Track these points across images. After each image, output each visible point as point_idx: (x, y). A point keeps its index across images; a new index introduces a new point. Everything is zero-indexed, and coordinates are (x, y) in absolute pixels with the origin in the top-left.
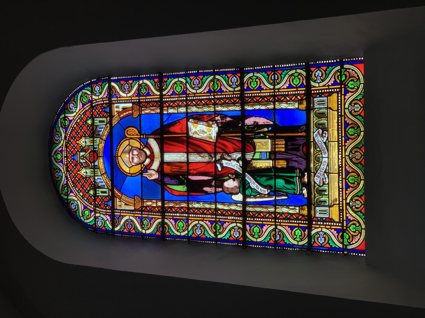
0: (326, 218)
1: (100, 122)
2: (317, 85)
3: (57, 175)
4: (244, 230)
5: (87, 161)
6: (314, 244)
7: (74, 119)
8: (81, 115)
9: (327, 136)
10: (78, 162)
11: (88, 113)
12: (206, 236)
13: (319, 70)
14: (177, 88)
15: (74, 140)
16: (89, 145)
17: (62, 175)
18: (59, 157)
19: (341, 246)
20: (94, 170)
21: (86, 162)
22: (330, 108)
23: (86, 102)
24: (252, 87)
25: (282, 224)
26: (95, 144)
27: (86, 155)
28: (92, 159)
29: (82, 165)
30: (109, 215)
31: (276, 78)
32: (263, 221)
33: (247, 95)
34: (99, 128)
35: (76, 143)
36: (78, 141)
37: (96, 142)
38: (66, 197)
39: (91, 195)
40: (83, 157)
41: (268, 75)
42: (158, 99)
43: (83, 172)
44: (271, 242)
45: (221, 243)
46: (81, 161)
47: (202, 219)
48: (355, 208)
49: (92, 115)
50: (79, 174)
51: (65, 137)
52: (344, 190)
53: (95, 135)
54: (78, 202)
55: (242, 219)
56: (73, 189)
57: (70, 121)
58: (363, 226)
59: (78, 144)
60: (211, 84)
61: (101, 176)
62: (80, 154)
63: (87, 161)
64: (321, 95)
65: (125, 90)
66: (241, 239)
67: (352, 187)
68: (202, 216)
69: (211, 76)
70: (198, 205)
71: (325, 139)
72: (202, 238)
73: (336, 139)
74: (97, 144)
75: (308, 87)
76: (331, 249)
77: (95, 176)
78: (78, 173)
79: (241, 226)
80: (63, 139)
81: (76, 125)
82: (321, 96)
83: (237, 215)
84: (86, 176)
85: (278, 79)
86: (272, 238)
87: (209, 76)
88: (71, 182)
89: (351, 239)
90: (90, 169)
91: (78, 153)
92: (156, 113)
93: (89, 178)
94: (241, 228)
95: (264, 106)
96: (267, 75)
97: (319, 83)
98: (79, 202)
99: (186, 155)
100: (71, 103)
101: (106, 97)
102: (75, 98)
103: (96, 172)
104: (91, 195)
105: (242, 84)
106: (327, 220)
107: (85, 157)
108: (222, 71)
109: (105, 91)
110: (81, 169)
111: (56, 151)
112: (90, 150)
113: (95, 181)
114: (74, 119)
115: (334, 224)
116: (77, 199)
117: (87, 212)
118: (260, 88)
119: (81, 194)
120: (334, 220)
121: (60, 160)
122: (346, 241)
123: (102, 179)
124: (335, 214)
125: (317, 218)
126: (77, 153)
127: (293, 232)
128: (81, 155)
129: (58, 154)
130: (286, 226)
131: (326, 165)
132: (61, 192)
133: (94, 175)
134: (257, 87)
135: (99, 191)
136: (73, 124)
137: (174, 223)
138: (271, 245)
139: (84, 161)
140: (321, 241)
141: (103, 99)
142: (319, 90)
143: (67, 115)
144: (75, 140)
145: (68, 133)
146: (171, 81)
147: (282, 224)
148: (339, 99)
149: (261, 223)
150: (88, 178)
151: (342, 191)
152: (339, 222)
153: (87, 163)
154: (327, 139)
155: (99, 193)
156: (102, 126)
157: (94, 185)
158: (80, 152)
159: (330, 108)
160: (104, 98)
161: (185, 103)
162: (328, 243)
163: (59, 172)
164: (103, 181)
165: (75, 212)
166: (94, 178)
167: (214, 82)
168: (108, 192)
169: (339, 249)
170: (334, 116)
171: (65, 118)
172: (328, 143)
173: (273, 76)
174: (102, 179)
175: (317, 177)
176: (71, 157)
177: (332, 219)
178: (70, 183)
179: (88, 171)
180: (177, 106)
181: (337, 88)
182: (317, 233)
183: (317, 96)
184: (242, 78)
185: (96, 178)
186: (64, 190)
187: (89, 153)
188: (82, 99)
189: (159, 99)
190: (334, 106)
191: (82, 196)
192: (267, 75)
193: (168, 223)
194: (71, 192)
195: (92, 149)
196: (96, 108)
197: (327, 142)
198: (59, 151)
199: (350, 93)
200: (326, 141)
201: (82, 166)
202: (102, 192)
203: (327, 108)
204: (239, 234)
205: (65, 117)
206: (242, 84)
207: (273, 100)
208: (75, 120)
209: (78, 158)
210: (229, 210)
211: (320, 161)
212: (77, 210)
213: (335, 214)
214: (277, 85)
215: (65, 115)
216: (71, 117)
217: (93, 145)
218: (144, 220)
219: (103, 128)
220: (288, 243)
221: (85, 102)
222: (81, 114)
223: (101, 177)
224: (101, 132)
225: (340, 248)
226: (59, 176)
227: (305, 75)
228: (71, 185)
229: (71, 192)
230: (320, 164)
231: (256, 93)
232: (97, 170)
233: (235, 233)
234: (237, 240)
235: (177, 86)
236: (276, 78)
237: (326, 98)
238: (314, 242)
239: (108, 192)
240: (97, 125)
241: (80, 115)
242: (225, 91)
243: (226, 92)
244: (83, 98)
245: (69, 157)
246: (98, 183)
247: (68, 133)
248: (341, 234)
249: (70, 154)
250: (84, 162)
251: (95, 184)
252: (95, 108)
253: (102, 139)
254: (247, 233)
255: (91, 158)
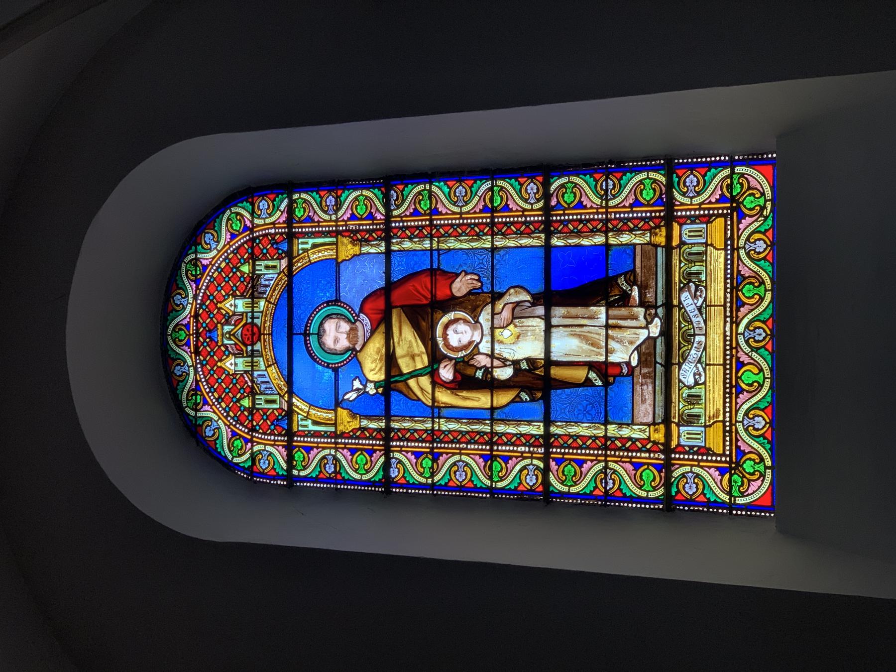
0: (700, 447)
1: (267, 267)
2: (687, 201)
3: (178, 371)
4: (546, 471)
5: (238, 342)
6: (596, 491)
7: (213, 263)
8: (228, 254)
9: (704, 296)
10: (219, 344)
11: (242, 250)
12: (624, 492)
13: (532, 182)
14: (359, 207)
15: (212, 301)
16: (243, 313)
17: (189, 370)
18: (182, 335)
19: (726, 498)
20: (252, 360)
21: (236, 344)
22: (712, 245)
23: (238, 231)
24: (645, 199)
25: (701, 464)
26: (255, 310)
27: (235, 330)
28: (248, 339)
29: (227, 348)
30: (283, 446)
31: (611, 187)
32: (373, 445)
33: (560, 217)
34: (265, 280)
35: (217, 307)
36: (221, 302)
37: (257, 307)
38: (192, 413)
39: (242, 408)
40: (230, 335)
41: (596, 181)
42: (540, 218)
43: (228, 364)
44: (597, 492)
45: (620, 504)
46: (226, 342)
47: (399, 449)
48: (753, 429)
49: (252, 254)
50: (221, 367)
51: (195, 297)
52: (734, 396)
53: (256, 294)
54: (220, 422)
55: (543, 451)
56: (210, 397)
57: (205, 267)
58: (769, 463)
59: (220, 309)
60: (488, 197)
61: (266, 370)
62: (222, 329)
63: (238, 342)
64: (694, 219)
65: (261, 212)
66: (541, 489)
67: (748, 392)
68: (316, 440)
69: (725, 168)
70: (529, 427)
71: (701, 300)
72: (269, 475)
73: (720, 302)
74: (258, 310)
75: (669, 204)
76: (709, 504)
77: (253, 370)
78: (219, 364)
79: (541, 465)
80: (191, 302)
81: (218, 272)
82: (693, 222)
83: (613, 447)
84: (235, 371)
85: (614, 188)
86: (599, 486)
87: (484, 181)
88: (205, 383)
89: (746, 486)
90: (243, 357)
91: (219, 325)
92: (517, 247)
93: (242, 375)
94: (541, 468)
95: (465, 244)
96: (319, 197)
97: (692, 198)
98: (222, 423)
99: (605, 331)
100: (208, 233)
101: (284, 222)
102: (216, 224)
103: (255, 364)
104: (242, 408)
105: (547, 196)
106: (702, 451)
107: (233, 335)
108: (704, 162)
109: (716, 187)
110: (225, 357)
111: (177, 325)
112: (244, 321)
113: (252, 381)
114: (213, 263)
115: (707, 458)
116: (216, 416)
117: (238, 443)
118: (580, 205)
119: (223, 405)
120: (713, 451)
121: (184, 342)
122: (737, 490)
123: (267, 375)
124: (715, 440)
125: (683, 446)
126: (216, 326)
127: (638, 474)
128: (225, 331)
129: (181, 329)
130: (710, 467)
131: (702, 349)
132: (185, 404)
133: (252, 368)
134: (576, 202)
135: (261, 399)
136: (212, 272)
137: (415, 461)
138: (597, 498)
139: (232, 342)
140: (690, 490)
141: (402, 217)
142: (690, 210)
143: (199, 256)
144: (216, 302)
145: (202, 287)
146: (716, 175)
147: (701, 464)
148: (729, 225)
149: (371, 447)
150: (239, 376)
151: (731, 398)
152: (724, 455)
153: (237, 347)
154: (705, 300)
155: (261, 404)
156: (270, 276)
157: (252, 388)
158: (223, 325)
159: (712, 245)
160: (406, 216)
161: (610, 226)
162: (619, 488)
163: (182, 364)
164: (270, 381)
165: (213, 442)
166: (252, 375)
167: (732, 178)
168: (278, 402)
169: (722, 505)
170: (718, 260)
171: (196, 262)
172: (706, 308)
173: (604, 183)
174: (267, 375)
175: (683, 372)
176: (206, 334)
177: (709, 449)
178: (204, 388)
179: (240, 361)
180: (360, 241)
181: (723, 209)
182: (683, 475)
183: (688, 222)
184: (546, 185)
185: (256, 374)
186: (191, 400)
187: (244, 326)
188: (231, 225)
189: (543, 218)
190: (719, 241)
191: (224, 409)
192: (594, 181)
193: (470, 465)
194: (205, 402)
195: (250, 320)
196: (260, 241)
197: (704, 306)
198: (182, 324)
199: (747, 218)
200: (702, 304)
201: (227, 353)
202: (268, 402)
203: (706, 244)
204: (537, 479)
205: (197, 259)
206: (547, 196)
207: (604, 229)
208: (214, 265)
209: (218, 335)
210: (467, 432)
211: (691, 342)
212: (217, 439)
213: (715, 440)
214: (611, 199)
215: (196, 256)
216: (207, 259)
217: (253, 312)
218: (296, 452)
219: (272, 280)
220: (346, 478)
221: (236, 230)
222: (229, 251)
223: (265, 373)
224: (269, 286)
225: (724, 502)
226: (183, 372)
227: (664, 183)
228: (205, 389)
229: (205, 402)
230: (690, 346)
231: (573, 215)
232: (258, 358)
233: (528, 477)
234: (531, 491)
235: (359, 205)
236: (611, 187)
237: (705, 226)
238: (678, 492)
239: (278, 402)
240: (260, 275)
241: (227, 253)
242: (444, 212)
243: (447, 214)
244: (233, 223)
245: (202, 334)
246: (259, 384)
247: (202, 287)
248: (727, 476)
249: (204, 328)
250: (230, 345)
251: (252, 385)
252: (257, 241)
253: (270, 303)
254: (551, 475)
255: (247, 337)
